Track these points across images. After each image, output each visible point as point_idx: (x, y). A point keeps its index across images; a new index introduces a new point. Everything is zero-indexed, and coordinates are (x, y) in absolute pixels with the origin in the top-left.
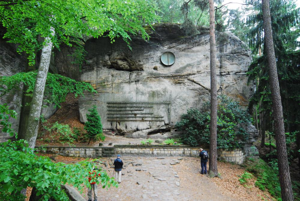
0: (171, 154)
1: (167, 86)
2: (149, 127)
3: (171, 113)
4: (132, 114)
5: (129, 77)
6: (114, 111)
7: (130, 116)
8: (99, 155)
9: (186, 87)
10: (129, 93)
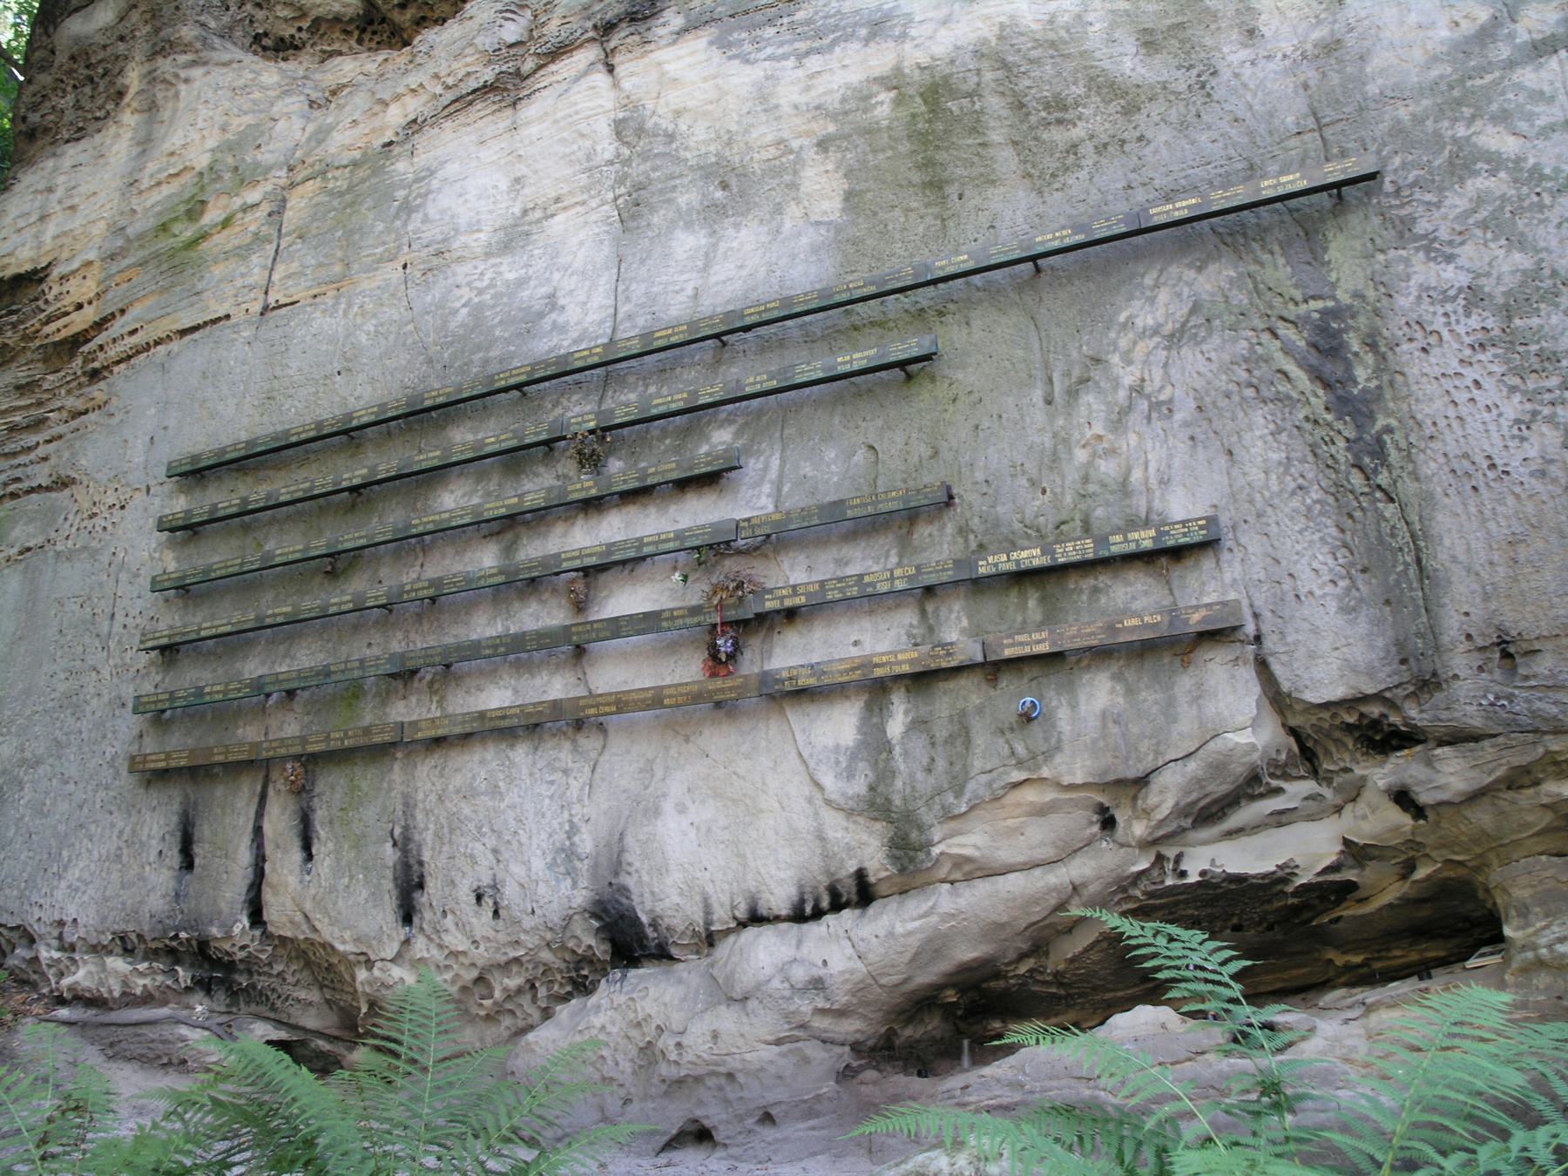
3: (1431, 407)
4: (530, 584)
10: (513, 238)
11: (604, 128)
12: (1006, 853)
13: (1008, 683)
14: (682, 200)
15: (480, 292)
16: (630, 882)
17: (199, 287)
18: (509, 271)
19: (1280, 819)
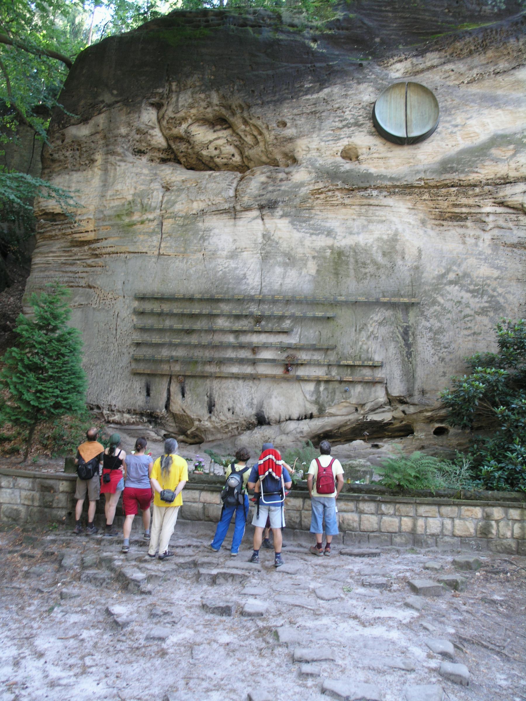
0: (413, 532)
1: (400, 230)
2: (314, 410)
3: (420, 349)
4: (242, 347)
5: (236, 190)
6: (161, 331)
7: (230, 354)
8: (55, 512)
9: (487, 236)
10: (233, 255)
11: (260, 235)
12: (338, 413)
13: (343, 384)
14: (278, 259)
15: (225, 268)
16: (264, 410)
17: (135, 240)
18: (232, 264)
19: (383, 412)
